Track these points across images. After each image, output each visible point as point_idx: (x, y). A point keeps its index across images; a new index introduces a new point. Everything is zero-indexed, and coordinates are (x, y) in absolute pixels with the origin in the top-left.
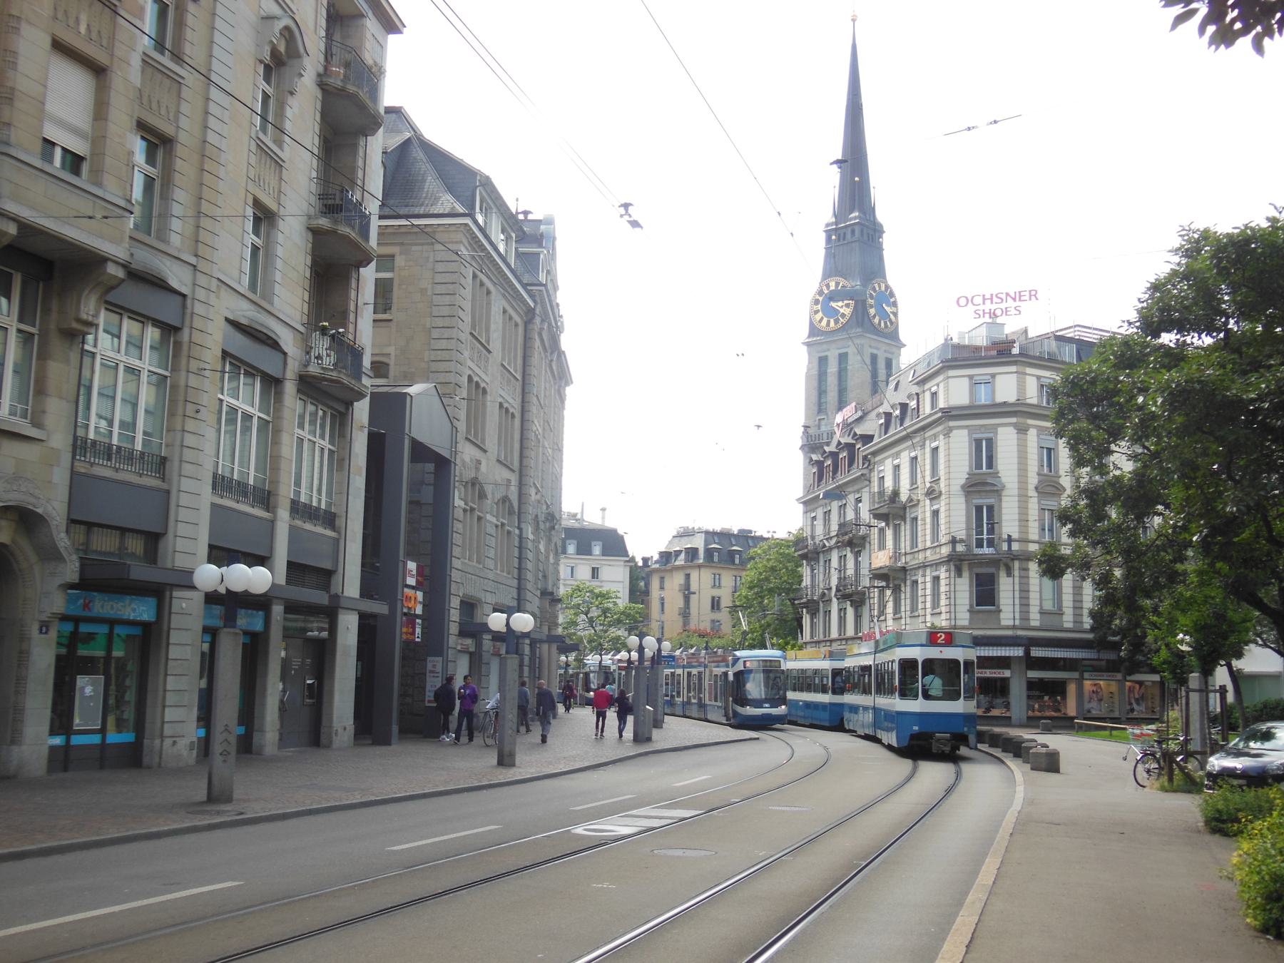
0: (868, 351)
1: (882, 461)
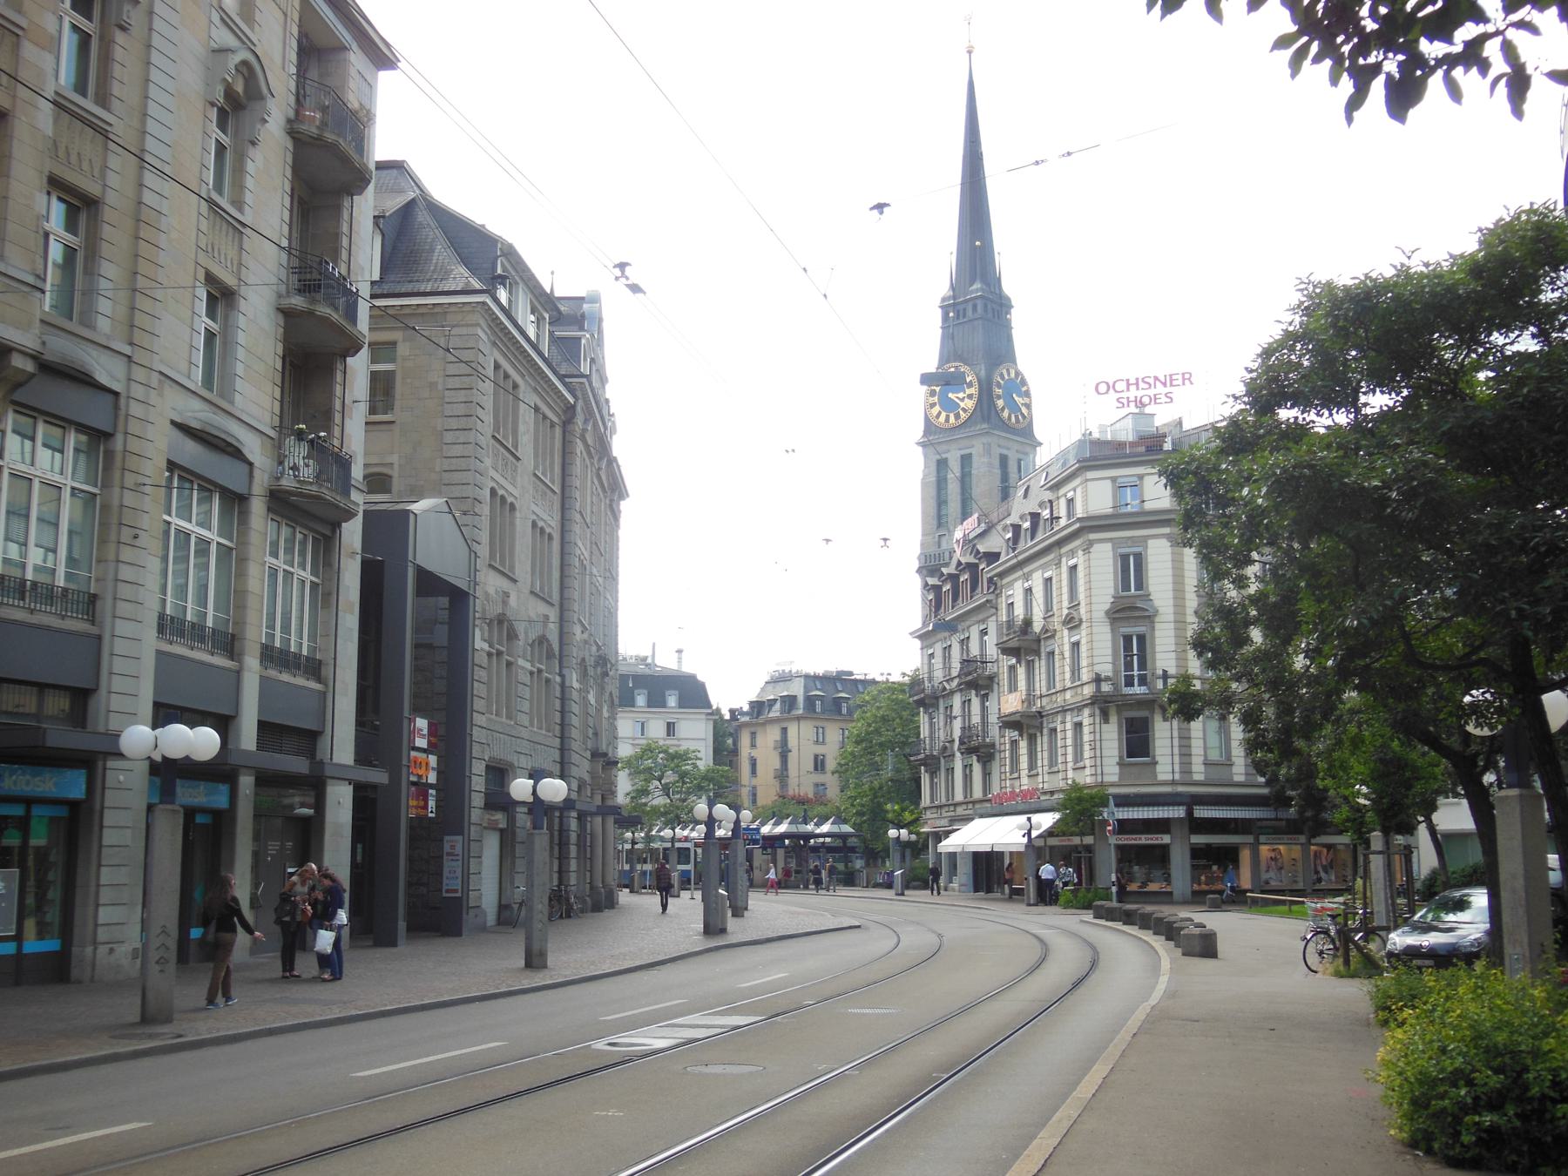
0: (997, 451)
1: (1011, 584)
